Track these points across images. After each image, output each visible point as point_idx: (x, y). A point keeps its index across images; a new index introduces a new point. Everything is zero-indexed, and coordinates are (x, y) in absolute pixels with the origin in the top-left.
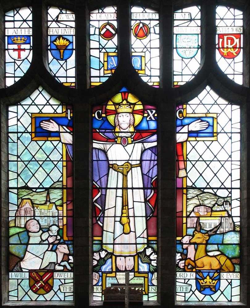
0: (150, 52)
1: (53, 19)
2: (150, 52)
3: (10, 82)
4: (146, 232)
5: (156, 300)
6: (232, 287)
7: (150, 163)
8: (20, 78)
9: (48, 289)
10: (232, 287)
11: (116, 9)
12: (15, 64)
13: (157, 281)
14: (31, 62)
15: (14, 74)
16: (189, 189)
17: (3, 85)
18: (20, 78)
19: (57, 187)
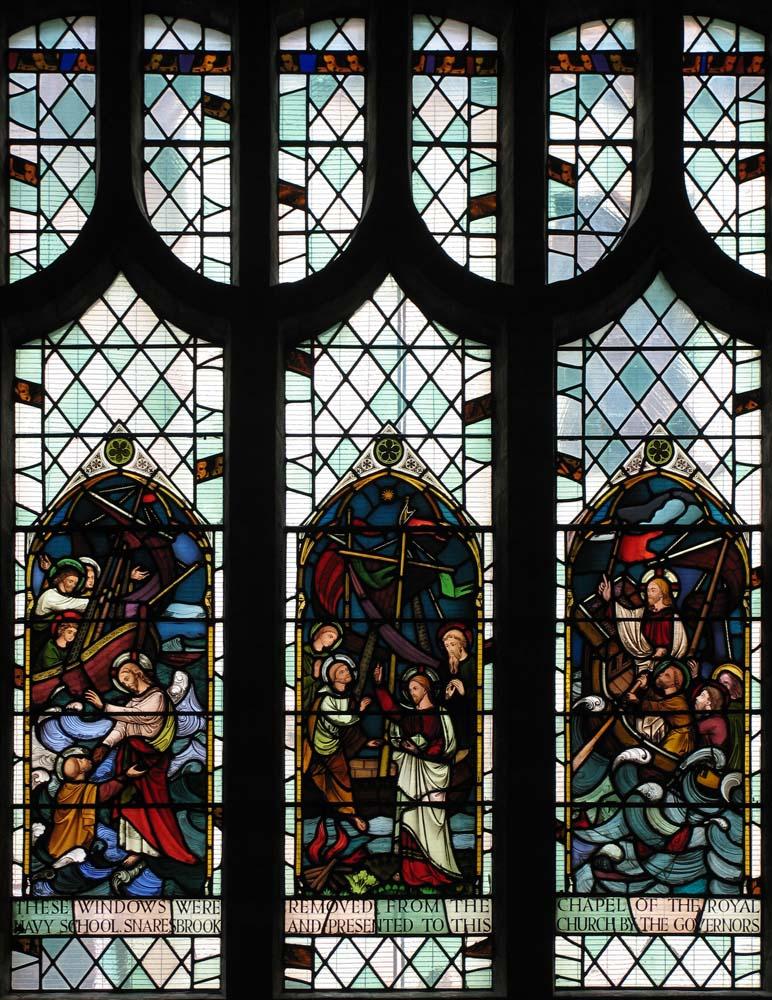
0: (201, 178)
1: (604, 134)
2: (201, 178)
3: (19, 272)
4: (144, 842)
5: (553, 77)
6: (195, 980)
7: (426, 789)
8: (579, 174)
9: (307, 350)
10: (195, 980)
11: (629, 159)
12: (461, 969)
13: (585, 22)
14: (692, 51)
15: (37, 130)
16: (476, 147)
17: (4, 282)
18: (579, 174)
19: (69, 618)
